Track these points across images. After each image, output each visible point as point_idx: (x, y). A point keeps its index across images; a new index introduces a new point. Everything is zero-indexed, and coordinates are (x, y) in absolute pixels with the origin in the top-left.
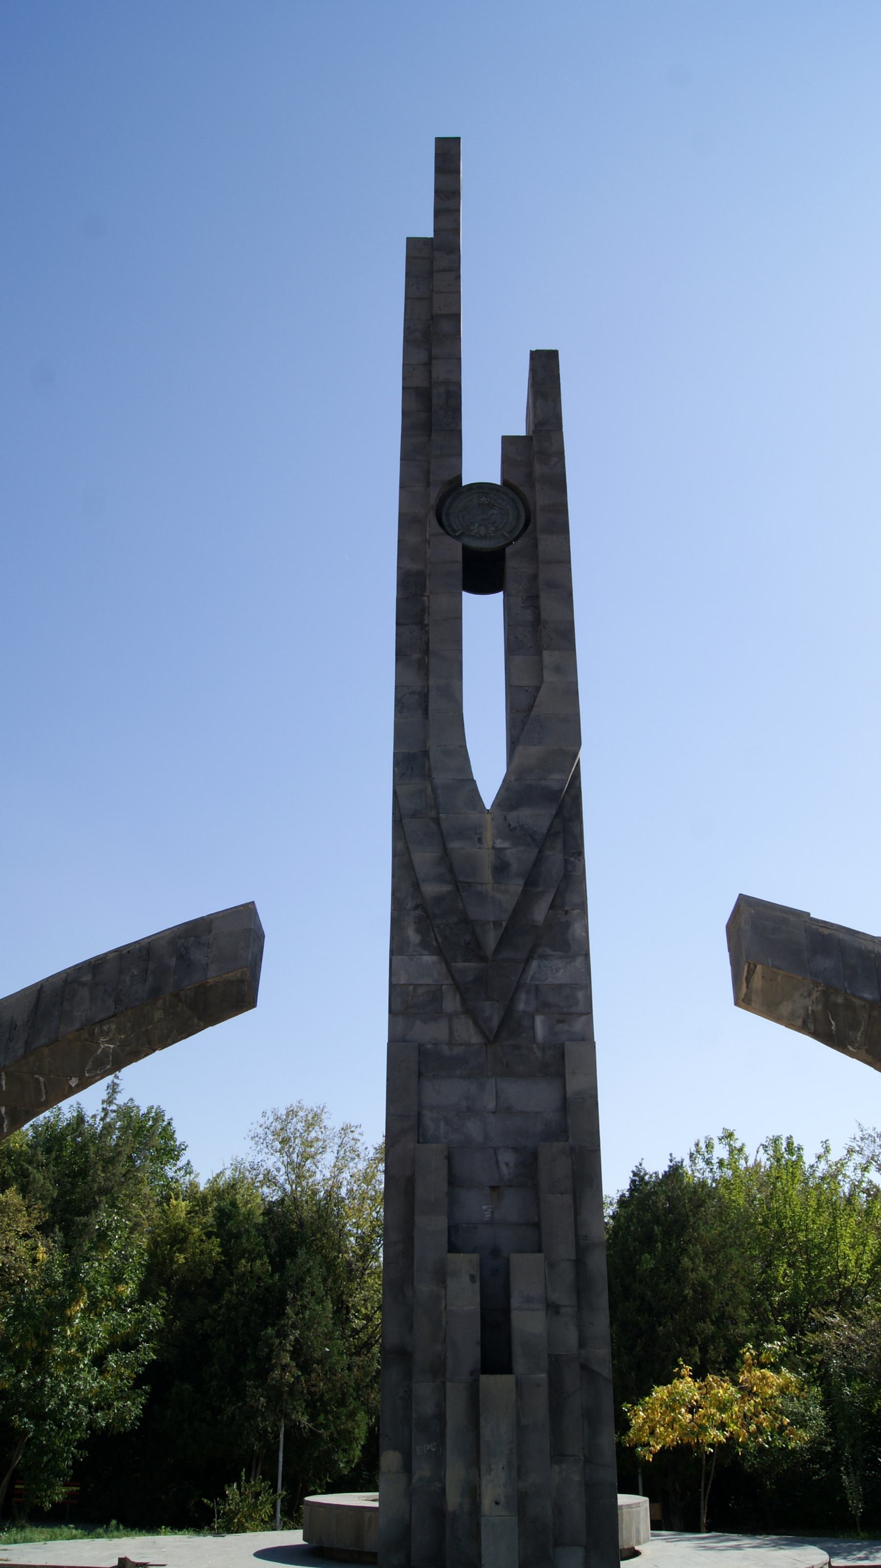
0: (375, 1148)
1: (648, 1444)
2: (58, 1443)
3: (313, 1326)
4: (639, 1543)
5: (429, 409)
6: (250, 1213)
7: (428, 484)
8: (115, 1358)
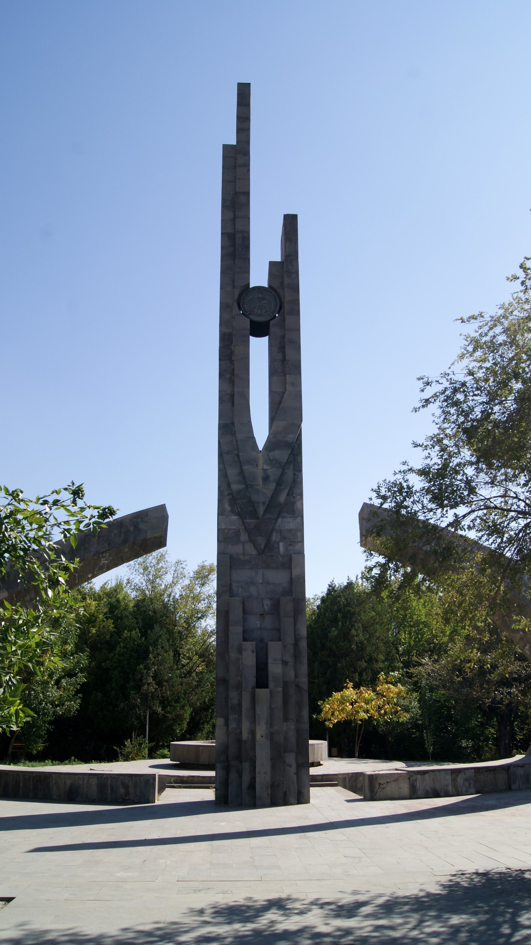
0: (194, 572)
1: (330, 720)
2: (39, 722)
3: (163, 664)
4: (322, 760)
5: (234, 245)
6: (126, 605)
7: (234, 287)
8: (66, 681)
